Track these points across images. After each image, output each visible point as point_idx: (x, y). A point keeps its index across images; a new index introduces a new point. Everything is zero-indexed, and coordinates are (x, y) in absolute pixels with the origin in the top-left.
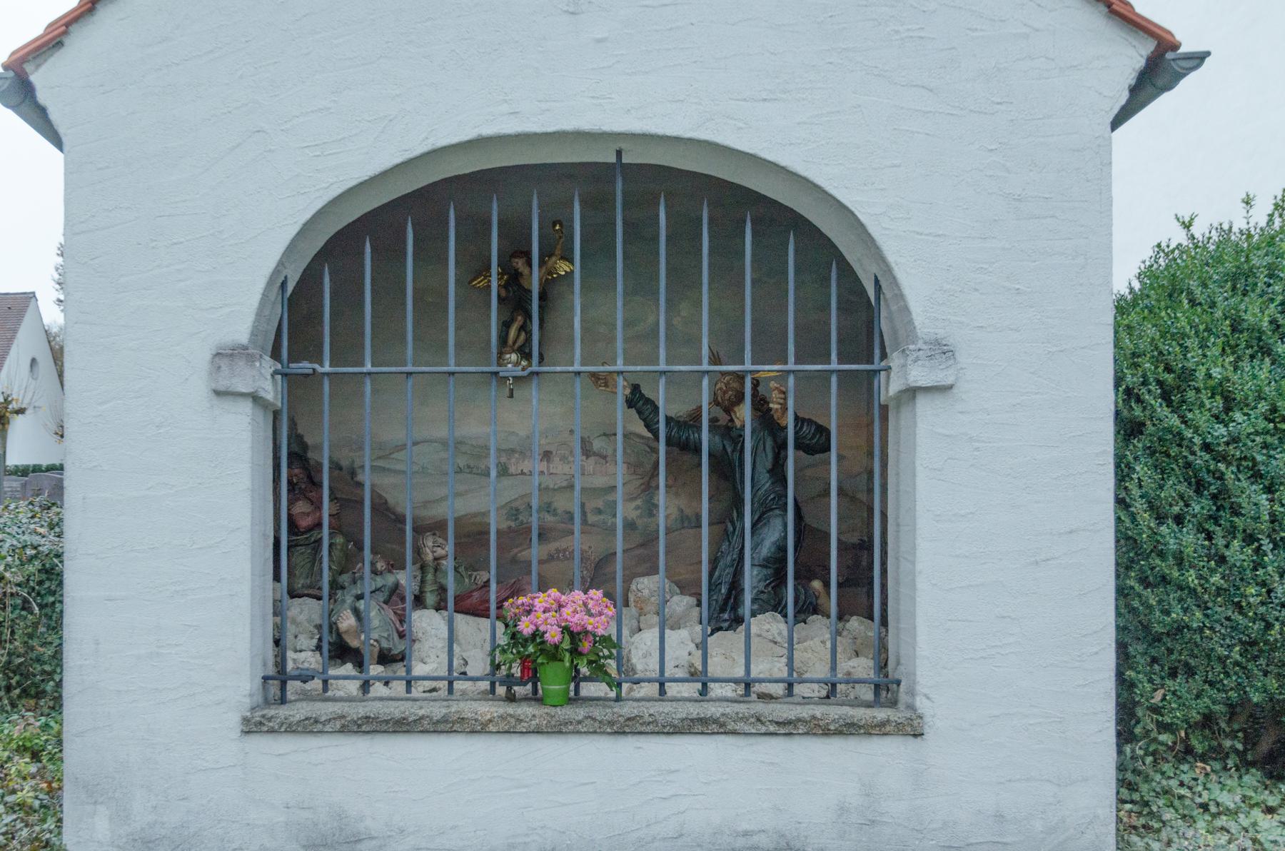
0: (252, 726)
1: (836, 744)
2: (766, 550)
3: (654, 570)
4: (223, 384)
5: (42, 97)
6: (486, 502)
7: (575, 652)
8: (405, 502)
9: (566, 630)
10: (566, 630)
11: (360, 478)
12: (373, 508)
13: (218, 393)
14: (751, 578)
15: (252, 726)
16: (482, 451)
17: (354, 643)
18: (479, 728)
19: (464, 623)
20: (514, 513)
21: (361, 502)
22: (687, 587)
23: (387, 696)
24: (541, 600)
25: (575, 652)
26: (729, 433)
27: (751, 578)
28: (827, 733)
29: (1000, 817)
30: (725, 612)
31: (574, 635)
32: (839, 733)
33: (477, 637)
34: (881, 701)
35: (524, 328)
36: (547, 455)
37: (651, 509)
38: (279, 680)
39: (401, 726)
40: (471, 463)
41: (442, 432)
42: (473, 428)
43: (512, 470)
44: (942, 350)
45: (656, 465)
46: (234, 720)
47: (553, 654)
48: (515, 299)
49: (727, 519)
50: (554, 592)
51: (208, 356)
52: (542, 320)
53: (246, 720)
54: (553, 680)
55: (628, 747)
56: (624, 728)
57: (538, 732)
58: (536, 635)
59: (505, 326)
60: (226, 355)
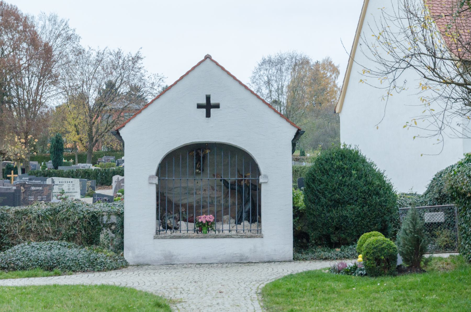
0: (155, 238)
1: (250, 239)
2: (247, 209)
3: (227, 214)
4: (151, 182)
5: (121, 135)
6: (192, 200)
7: (208, 225)
8: (174, 200)
9: (206, 221)
10: (206, 221)
11: (165, 195)
12: (168, 201)
13: (150, 183)
14: (244, 215)
15: (155, 238)
16: (192, 189)
17: (170, 226)
18: (192, 238)
19: (189, 224)
20: (198, 202)
21: (165, 200)
22: (234, 218)
23: (177, 233)
24: (202, 217)
25: (208, 225)
26: (240, 186)
27: (244, 215)
28: (248, 237)
29: (275, 250)
30: (239, 222)
31: (208, 222)
32: (250, 237)
33: (191, 226)
34: (259, 234)
35: (200, 164)
36: (205, 190)
37: (227, 201)
38: (158, 232)
39: (180, 237)
40: (190, 192)
41: (183, 185)
42: (190, 185)
43: (197, 193)
44: (266, 177)
45: (228, 191)
46: (152, 237)
47: (204, 225)
48: (198, 160)
49: (240, 204)
50: (204, 215)
51: (148, 177)
52: (203, 163)
53: (154, 237)
54: (204, 230)
55: (216, 240)
56: (216, 237)
57: (202, 238)
58: (202, 222)
59: (196, 164)
60: (151, 177)
